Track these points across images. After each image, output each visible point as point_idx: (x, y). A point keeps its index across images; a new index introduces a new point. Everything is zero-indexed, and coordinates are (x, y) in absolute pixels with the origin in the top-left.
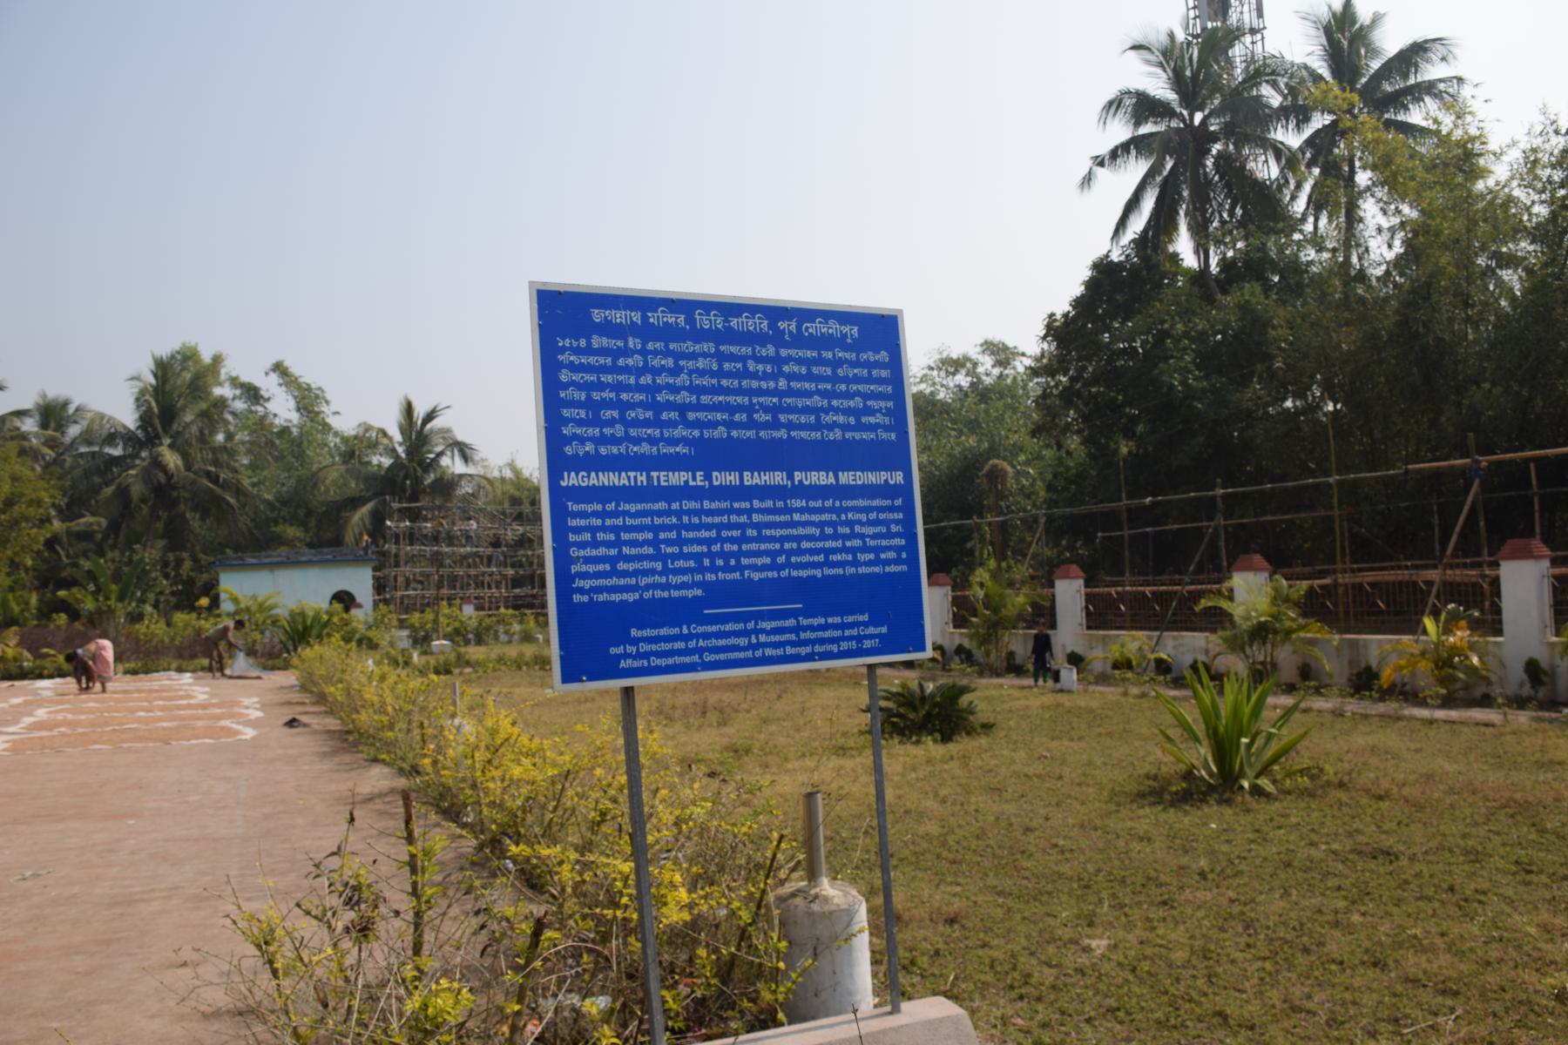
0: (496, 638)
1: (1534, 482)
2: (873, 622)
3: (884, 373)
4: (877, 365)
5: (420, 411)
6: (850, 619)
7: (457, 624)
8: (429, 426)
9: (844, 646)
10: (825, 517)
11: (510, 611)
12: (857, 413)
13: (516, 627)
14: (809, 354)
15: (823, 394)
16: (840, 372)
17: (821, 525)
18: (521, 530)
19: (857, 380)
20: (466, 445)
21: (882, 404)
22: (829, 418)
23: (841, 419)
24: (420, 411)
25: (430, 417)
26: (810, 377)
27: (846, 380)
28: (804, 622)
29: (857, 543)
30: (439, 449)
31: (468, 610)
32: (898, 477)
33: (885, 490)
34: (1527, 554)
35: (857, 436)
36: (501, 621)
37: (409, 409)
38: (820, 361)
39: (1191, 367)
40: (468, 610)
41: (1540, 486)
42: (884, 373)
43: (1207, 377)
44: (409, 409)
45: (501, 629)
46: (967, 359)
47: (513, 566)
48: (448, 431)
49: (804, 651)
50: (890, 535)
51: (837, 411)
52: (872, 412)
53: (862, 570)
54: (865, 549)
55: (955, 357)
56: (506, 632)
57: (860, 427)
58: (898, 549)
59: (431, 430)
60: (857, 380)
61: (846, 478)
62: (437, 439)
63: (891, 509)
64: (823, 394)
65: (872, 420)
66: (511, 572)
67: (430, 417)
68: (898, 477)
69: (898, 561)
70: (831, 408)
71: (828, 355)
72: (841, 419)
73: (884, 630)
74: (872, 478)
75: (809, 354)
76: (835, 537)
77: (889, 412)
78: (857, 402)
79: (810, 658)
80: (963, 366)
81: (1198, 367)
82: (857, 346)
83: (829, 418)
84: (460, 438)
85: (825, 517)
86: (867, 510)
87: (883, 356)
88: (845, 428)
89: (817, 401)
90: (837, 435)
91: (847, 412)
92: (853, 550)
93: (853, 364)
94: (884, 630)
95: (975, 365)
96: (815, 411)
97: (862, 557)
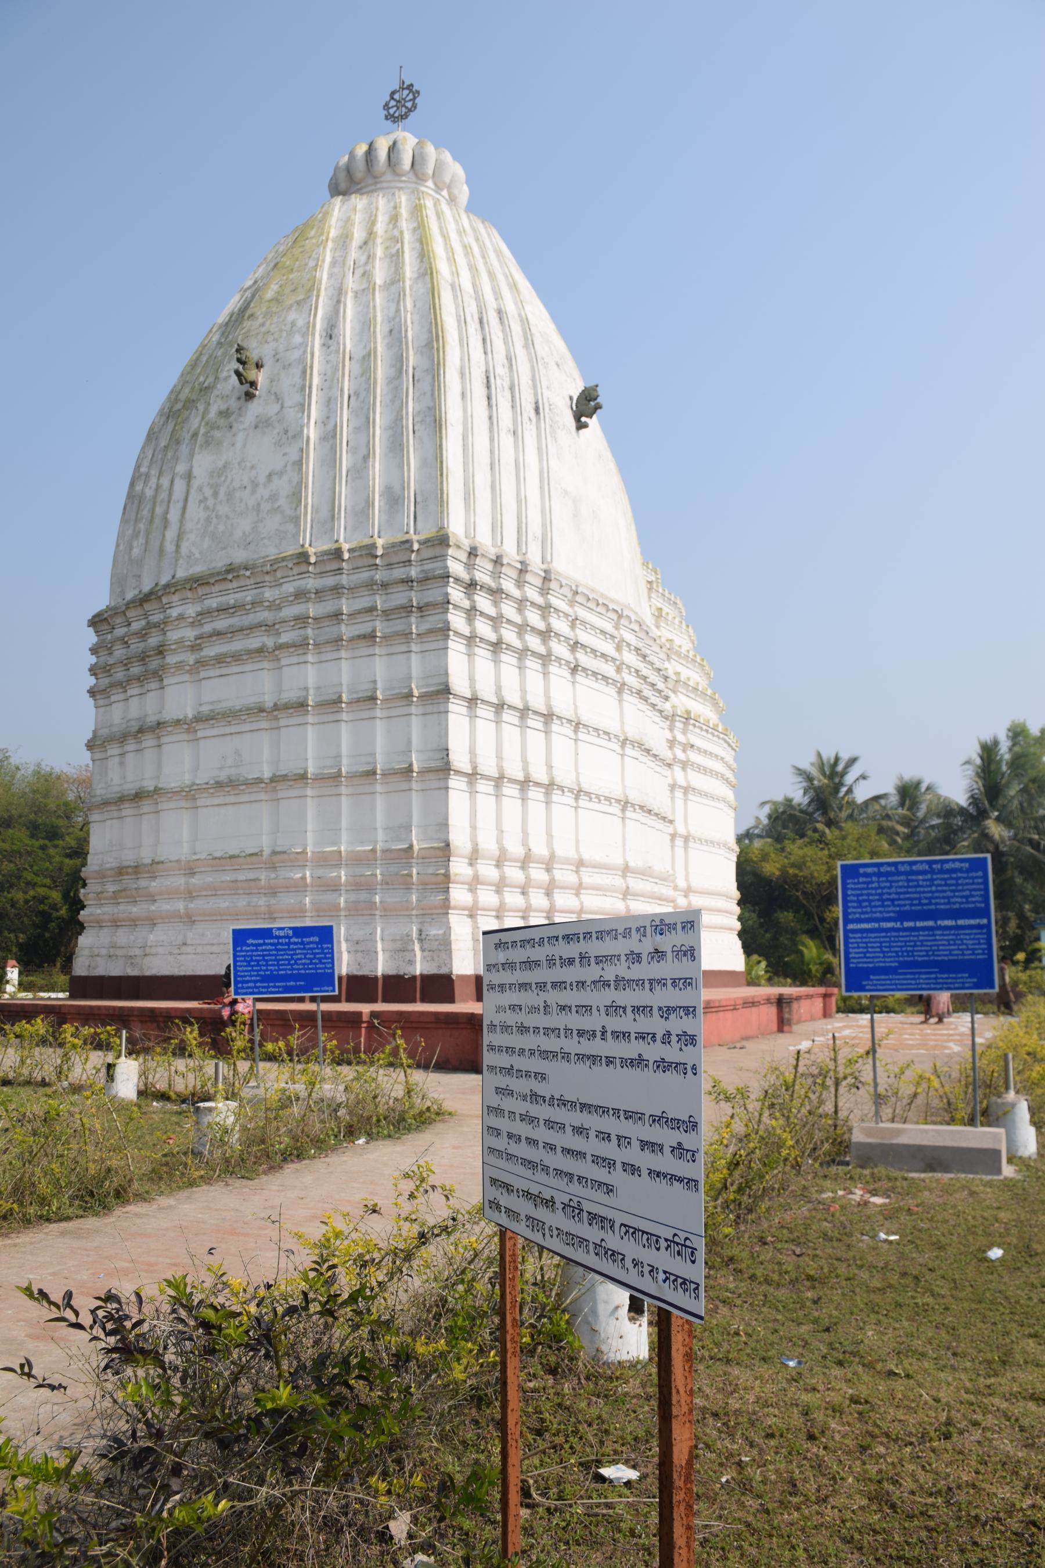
12: (966, 897)
26: (946, 885)
32: (985, 921)
33: (979, 927)
38: (951, 878)
57: (968, 902)
61: (960, 922)
68: (985, 921)
74: (972, 922)
78: (967, 893)
82: (968, 871)
87: (980, 874)
89: (949, 894)
90: (957, 906)
96: (948, 898)
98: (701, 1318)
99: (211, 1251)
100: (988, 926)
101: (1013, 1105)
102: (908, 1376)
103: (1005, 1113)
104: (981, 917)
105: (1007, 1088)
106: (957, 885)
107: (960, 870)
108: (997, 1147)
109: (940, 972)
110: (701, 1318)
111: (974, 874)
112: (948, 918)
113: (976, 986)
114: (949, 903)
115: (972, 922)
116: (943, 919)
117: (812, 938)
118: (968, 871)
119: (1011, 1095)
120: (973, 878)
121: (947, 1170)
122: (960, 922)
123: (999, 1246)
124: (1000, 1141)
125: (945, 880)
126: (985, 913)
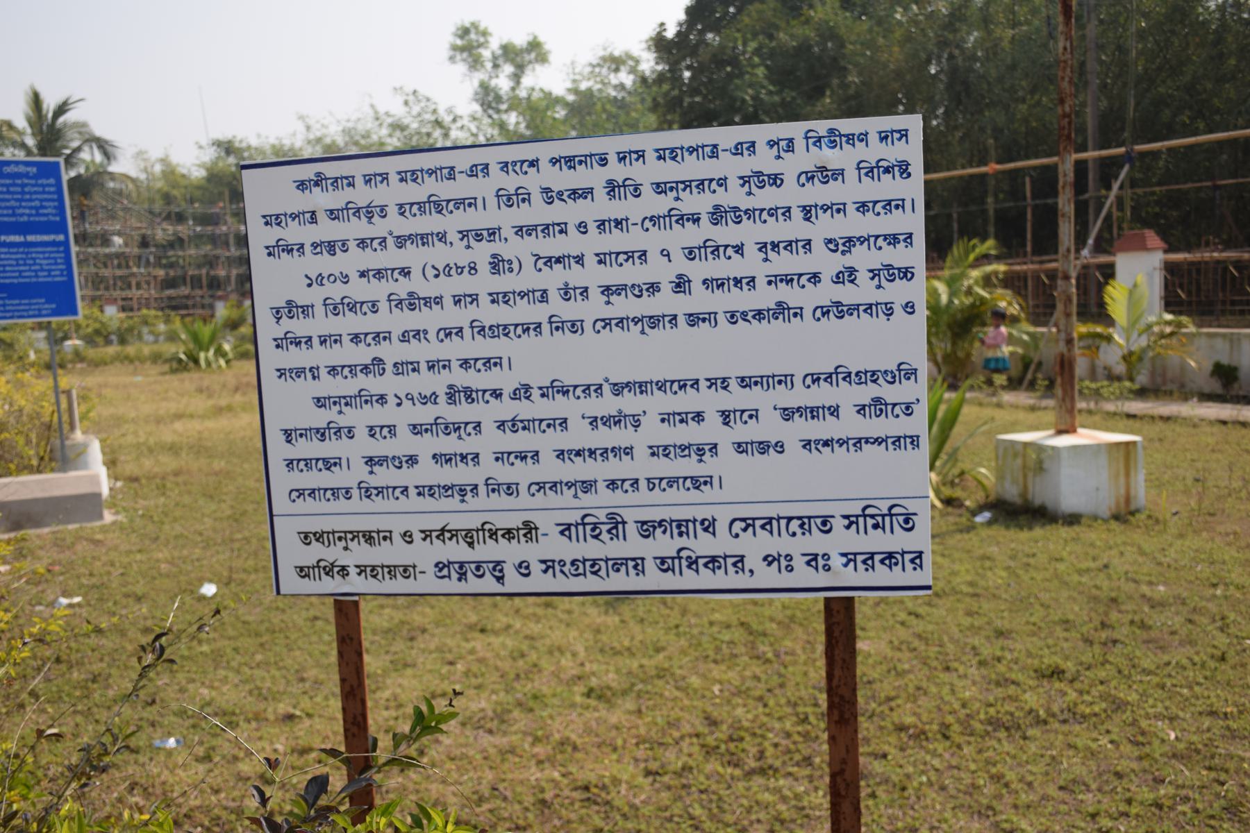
0: (140, 337)
1: (1028, 194)
2: (47, 302)
3: (52, 189)
4: (48, 185)
5: (50, 103)
6: (34, 301)
7: (97, 326)
8: (61, 120)
9: (31, 313)
10: (19, 256)
11: (153, 312)
12: (37, 208)
13: (162, 327)
14: (8, 181)
15: (17, 200)
16: (26, 189)
17: (17, 260)
18: (170, 229)
19: (36, 193)
20: (106, 142)
21: (51, 204)
22: (21, 211)
23: (27, 211)
24: (50, 103)
25: (62, 109)
26: (8, 192)
27: (30, 193)
28: (7, 302)
29: (37, 267)
30: (75, 144)
31: (111, 311)
32: (61, 237)
33: (54, 244)
34: (1142, 247)
35: (37, 219)
36: (145, 322)
37: (36, 100)
38: (14, 185)
39: (765, 83)
40: (111, 311)
41: (1034, 197)
42: (52, 189)
43: (779, 92)
44: (36, 100)
45: (145, 330)
46: (630, 57)
47: (165, 267)
48: (84, 125)
49: (8, 315)
50: (56, 264)
51: (25, 208)
52: (45, 208)
53: (41, 280)
54: (42, 270)
55: (617, 53)
56: (151, 332)
57: (38, 215)
58: (62, 270)
59: (65, 124)
60: (36, 193)
61: (30, 238)
62: (71, 134)
63: (58, 252)
64: (17, 200)
65: (45, 211)
66: (161, 273)
67: (62, 109)
68: (61, 237)
69: (62, 275)
70: (20, 207)
71: (19, 182)
72: (27, 211)
73: (54, 306)
74: (46, 238)
75: (8, 181)
76: (25, 265)
77: (55, 207)
78: (37, 203)
79: (12, 317)
80: (624, 63)
81: (773, 82)
82: (36, 177)
83: (21, 211)
84: (99, 132)
85: (19, 256)
86: (44, 253)
87: (52, 181)
88: (30, 215)
89: (13, 203)
90: (25, 219)
91: (31, 208)
92: (36, 271)
93: (33, 186)
94: (54, 306)
95: (637, 62)
96: (13, 208)
97: (40, 274)
98: (929, 588)
99: (1122, 554)
100: (66, 244)
101: (85, 446)
102: (309, 715)
103: (80, 454)
104: (57, 232)
105: (72, 427)
106: (23, 193)
107: (27, 175)
108: (95, 490)
109: (9, 298)
110: (929, 588)
111: (44, 181)
112: (15, 233)
113: (55, 313)
114: (14, 215)
115: (46, 238)
116: (8, 233)
117: (615, 97)
118: (36, 177)
119: (78, 436)
120: (43, 186)
121: (38, 524)
122: (30, 238)
123: (211, 581)
124: (98, 483)
125: (7, 186)
126: (61, 227)
